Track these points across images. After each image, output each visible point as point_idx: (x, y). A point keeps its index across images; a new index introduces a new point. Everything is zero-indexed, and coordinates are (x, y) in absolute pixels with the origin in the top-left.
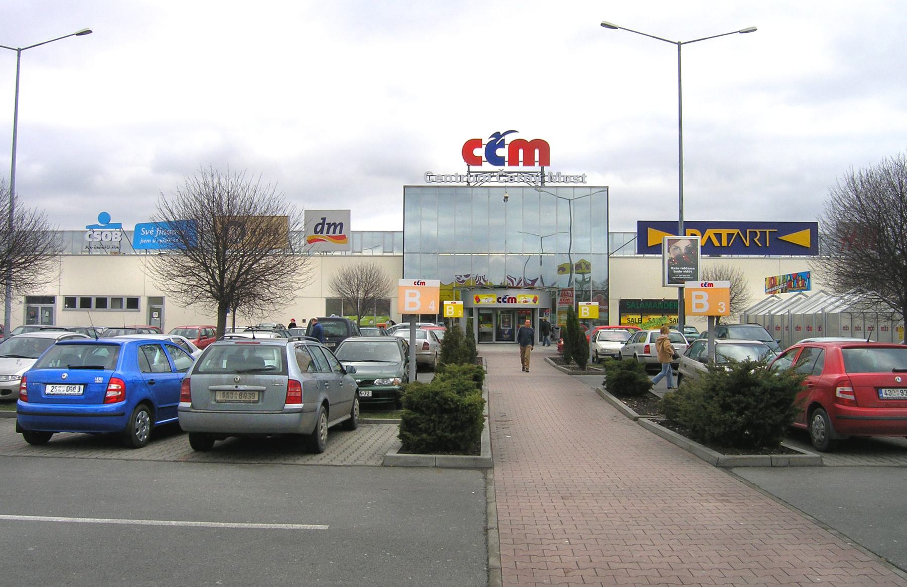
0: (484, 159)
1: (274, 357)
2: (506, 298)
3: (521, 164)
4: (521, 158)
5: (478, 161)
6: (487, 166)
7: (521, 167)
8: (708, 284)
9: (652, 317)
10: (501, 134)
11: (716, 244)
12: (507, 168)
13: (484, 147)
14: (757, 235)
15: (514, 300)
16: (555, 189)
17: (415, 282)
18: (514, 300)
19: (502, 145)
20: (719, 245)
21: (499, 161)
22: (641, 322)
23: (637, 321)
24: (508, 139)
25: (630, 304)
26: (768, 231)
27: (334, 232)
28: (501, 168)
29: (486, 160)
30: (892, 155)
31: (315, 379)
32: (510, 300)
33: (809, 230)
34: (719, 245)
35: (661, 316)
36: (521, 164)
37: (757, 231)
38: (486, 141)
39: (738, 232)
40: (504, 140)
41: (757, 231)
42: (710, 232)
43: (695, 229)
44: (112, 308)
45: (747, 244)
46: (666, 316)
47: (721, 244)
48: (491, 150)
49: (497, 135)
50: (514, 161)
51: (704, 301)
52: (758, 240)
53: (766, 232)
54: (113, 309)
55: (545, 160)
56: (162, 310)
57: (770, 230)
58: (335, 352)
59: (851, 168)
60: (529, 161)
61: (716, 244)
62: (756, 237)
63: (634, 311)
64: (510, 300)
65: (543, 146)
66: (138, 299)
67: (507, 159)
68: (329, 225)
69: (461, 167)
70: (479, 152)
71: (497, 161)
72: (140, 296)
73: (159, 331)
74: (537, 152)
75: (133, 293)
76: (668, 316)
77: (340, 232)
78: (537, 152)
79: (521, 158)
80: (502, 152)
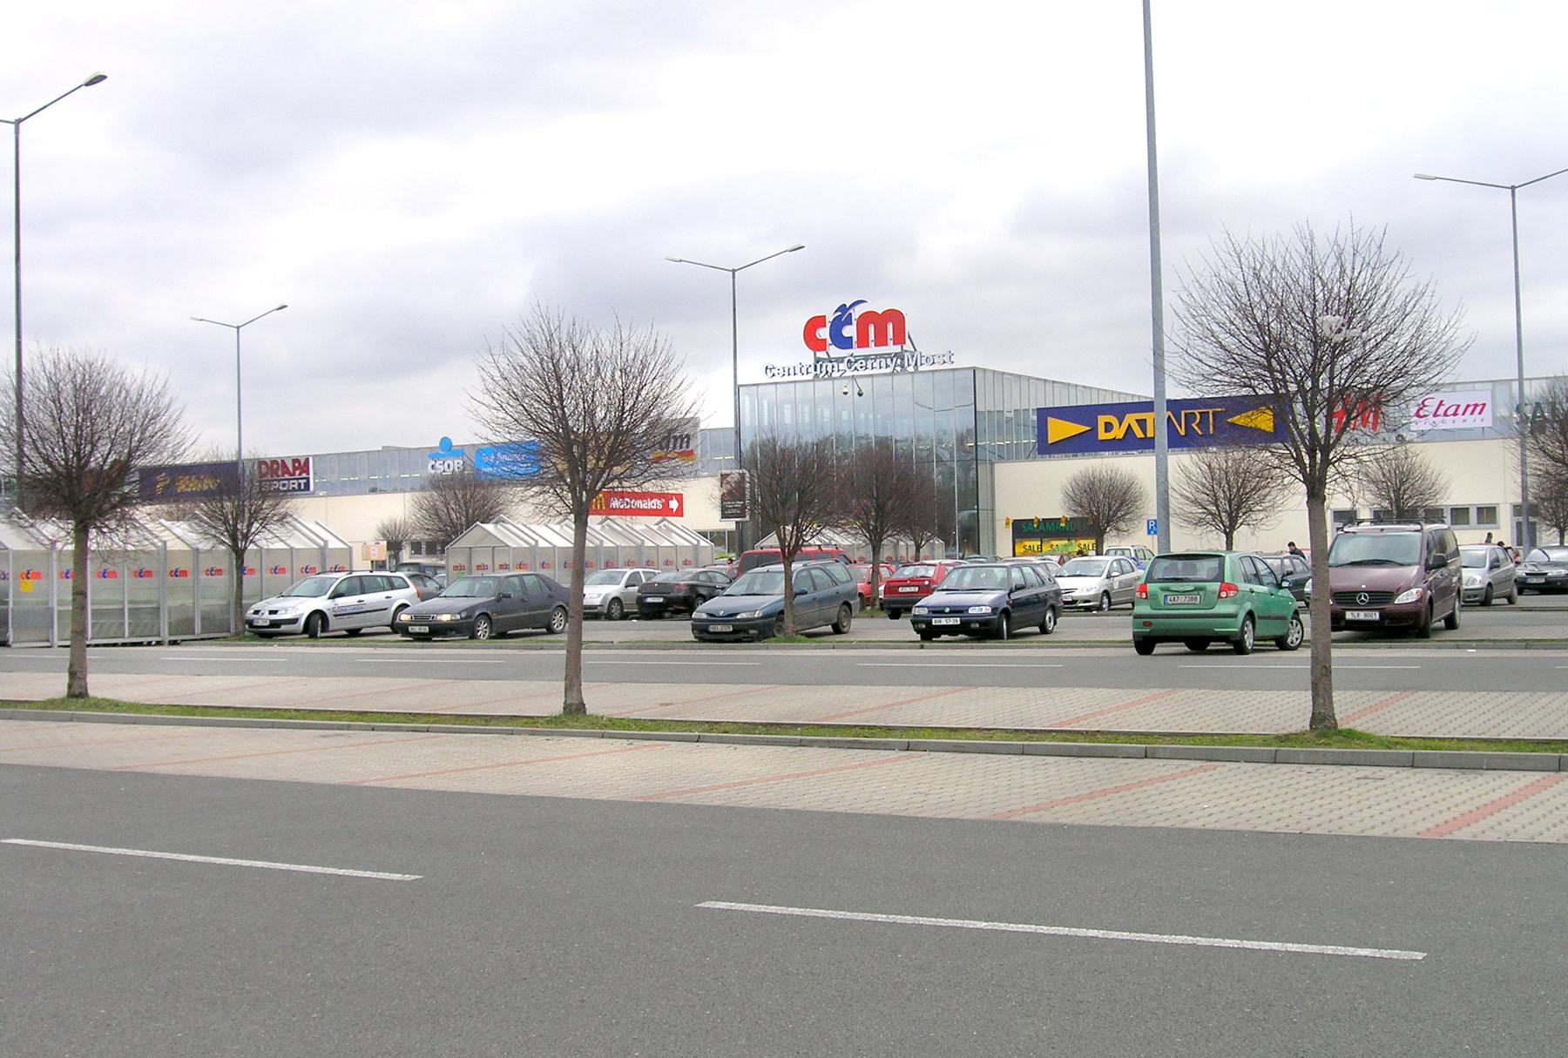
0: (829, 341)
4: (872, 336)
6: (835, 352)
7: (873, 350)
9: (1055, 543)
10: (848, 306)
11: (1139, 434)
13: (828, 325)
14: (1196, 418)
16: (774, 386)
20: (1143, 436)
22: (1041, 551)
23: (1036, 549)
24: (857, 313)
25: (1027, 526)
26: (1211, 411)
27: (681, 447)
28: (850, 351)
29: (831, 342)
32: (872, 329)
33: (1049, 419)
34: (1143, 436)
35: (1066, 542)
37: (1196, 412)
38: (830, 318)
39: (1169, 417)
40: (851, 314)
41: (1196, 412)
42: (1130, 419)
43: (1110, 414)
44: (1478, 523)
45: (1182, 433)
46: (1073, 541)
47: (1145, 434)
48: (838, 325)
49: (843, 308)
50: (863, 343)
51: (376, 552)
52: (1197, 425)
53: (1208, 412)
54: (1482, 526)
55: (900, 338)
56: (1465, 526)
57: (1187, 411)
58: (323, 634)
59: (1428, 314)
60: (881, 340)
61: (1139, 434)
62: (1193, 422)
63: (1031, 535)
64: (872, 329)
65: (896, 317)
66: (1495, 508)
67: (855, 339)
68: (676, 438)
69: (808, 357)
70: (824, 333)
71: (845, 343)
72: (1498, 504)
74: (890, 327)
75: (1485, 500)
76: (1076, 540)
77: (688, 447)
78: (890, 327)
79: (872, 336)
80: (850, 331)
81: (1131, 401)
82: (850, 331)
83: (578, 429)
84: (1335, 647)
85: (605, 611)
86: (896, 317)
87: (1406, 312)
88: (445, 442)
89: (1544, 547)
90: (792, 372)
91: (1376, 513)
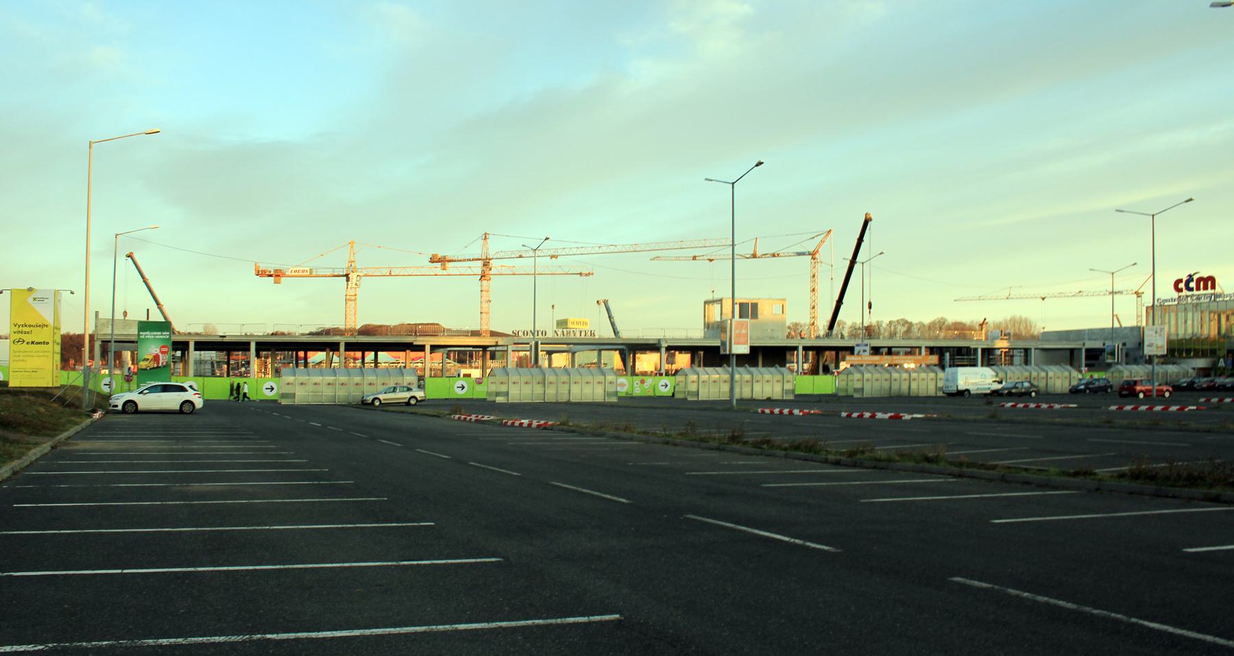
0: (1184, 288)
1: (910, 338)
2: (1192, 280)
3: (1202, 290)
5: (1181, 290)
6: (1185, 293)
8: (1199, 280)
12: (1195, 292)
15: (1209, 283)
16: (731, 243)
17: (1180, 281)
18: (1209, 283)
19: (1192, 280)
21: (1191, 289)
24: (1195, 278)
27: (538, 335)
30: (871, 301)
31: (159, 398)
32: (1202, 283)
36: (1202, 290)
49: (1190, 276)
50: (1198, 288)
55: (1213, 287)
60: (1206, 288)
64: (1202, 283)
65: (1212, 279)
69: (1175, 295)
70: (1182, 285)
73: (735, 344)
80: (1193, 285)
81: (202, 352)
82: (1193, 285)
83: (575, 335)
84: (133, 335)
85: (840, 353)
86: (1212, 279)
87: (222, 356)
88: (246, 335)
89: (513, 336)
90: (540, 333)
91: (868, 327)
